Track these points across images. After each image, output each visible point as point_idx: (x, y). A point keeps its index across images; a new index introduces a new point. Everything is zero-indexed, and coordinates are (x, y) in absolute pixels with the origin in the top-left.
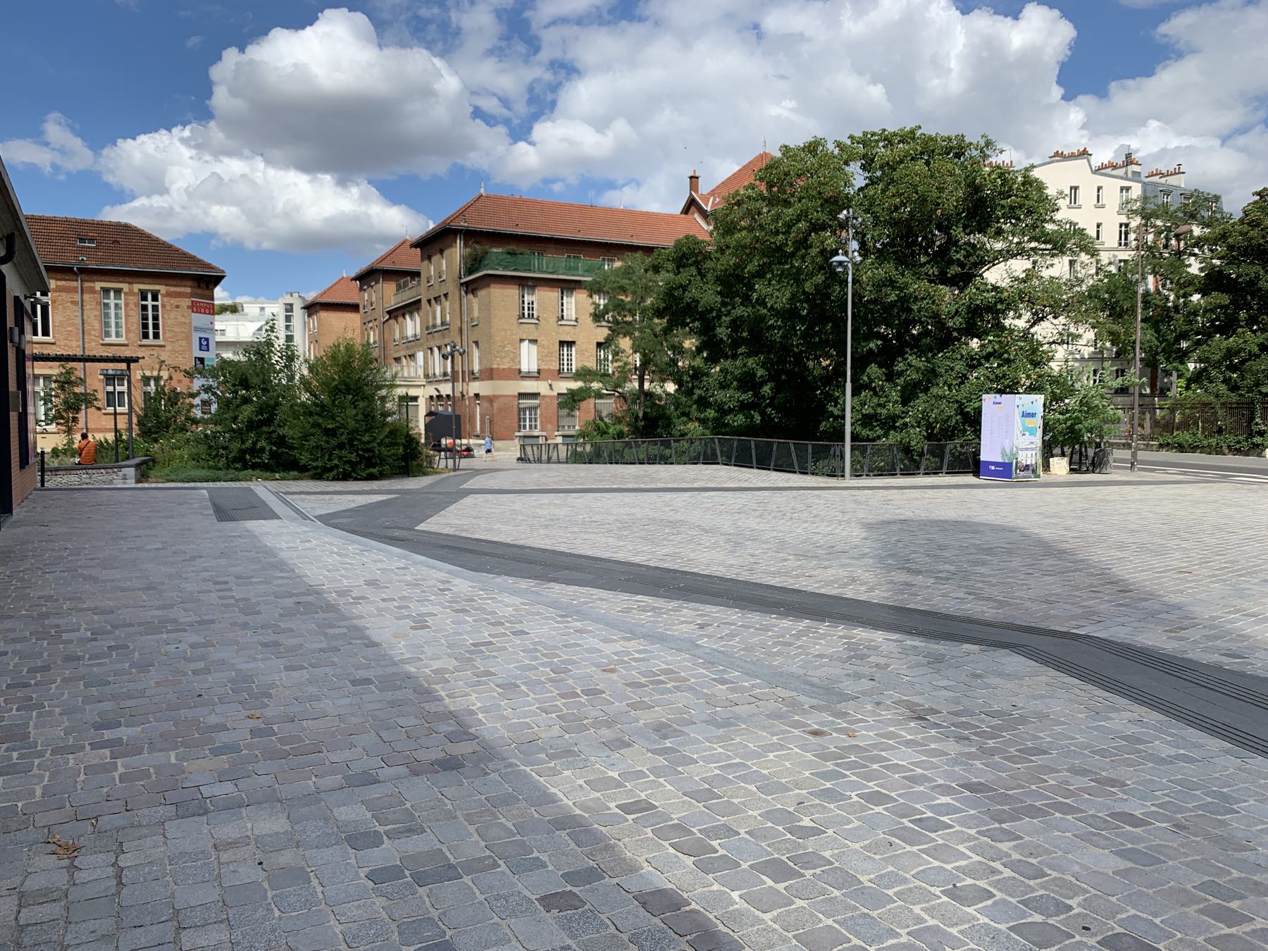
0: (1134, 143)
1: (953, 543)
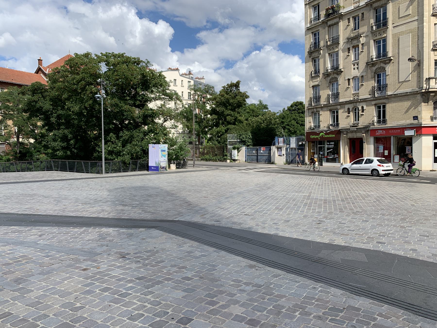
0: (192, 68)
1: (139, 194)
